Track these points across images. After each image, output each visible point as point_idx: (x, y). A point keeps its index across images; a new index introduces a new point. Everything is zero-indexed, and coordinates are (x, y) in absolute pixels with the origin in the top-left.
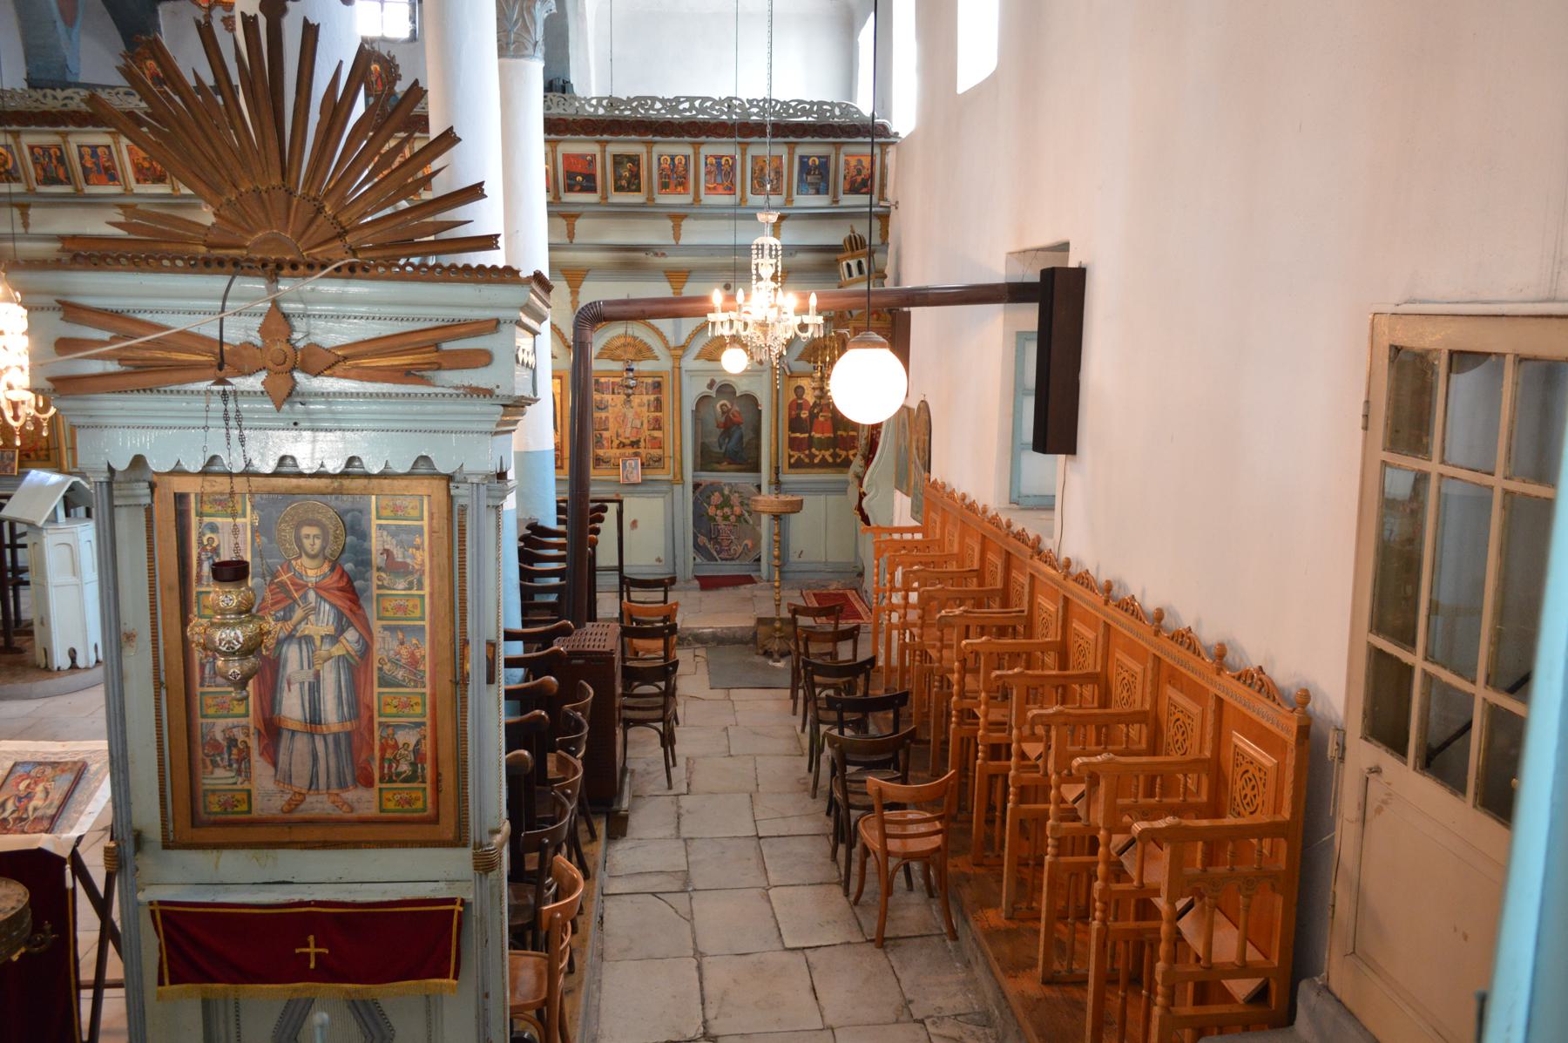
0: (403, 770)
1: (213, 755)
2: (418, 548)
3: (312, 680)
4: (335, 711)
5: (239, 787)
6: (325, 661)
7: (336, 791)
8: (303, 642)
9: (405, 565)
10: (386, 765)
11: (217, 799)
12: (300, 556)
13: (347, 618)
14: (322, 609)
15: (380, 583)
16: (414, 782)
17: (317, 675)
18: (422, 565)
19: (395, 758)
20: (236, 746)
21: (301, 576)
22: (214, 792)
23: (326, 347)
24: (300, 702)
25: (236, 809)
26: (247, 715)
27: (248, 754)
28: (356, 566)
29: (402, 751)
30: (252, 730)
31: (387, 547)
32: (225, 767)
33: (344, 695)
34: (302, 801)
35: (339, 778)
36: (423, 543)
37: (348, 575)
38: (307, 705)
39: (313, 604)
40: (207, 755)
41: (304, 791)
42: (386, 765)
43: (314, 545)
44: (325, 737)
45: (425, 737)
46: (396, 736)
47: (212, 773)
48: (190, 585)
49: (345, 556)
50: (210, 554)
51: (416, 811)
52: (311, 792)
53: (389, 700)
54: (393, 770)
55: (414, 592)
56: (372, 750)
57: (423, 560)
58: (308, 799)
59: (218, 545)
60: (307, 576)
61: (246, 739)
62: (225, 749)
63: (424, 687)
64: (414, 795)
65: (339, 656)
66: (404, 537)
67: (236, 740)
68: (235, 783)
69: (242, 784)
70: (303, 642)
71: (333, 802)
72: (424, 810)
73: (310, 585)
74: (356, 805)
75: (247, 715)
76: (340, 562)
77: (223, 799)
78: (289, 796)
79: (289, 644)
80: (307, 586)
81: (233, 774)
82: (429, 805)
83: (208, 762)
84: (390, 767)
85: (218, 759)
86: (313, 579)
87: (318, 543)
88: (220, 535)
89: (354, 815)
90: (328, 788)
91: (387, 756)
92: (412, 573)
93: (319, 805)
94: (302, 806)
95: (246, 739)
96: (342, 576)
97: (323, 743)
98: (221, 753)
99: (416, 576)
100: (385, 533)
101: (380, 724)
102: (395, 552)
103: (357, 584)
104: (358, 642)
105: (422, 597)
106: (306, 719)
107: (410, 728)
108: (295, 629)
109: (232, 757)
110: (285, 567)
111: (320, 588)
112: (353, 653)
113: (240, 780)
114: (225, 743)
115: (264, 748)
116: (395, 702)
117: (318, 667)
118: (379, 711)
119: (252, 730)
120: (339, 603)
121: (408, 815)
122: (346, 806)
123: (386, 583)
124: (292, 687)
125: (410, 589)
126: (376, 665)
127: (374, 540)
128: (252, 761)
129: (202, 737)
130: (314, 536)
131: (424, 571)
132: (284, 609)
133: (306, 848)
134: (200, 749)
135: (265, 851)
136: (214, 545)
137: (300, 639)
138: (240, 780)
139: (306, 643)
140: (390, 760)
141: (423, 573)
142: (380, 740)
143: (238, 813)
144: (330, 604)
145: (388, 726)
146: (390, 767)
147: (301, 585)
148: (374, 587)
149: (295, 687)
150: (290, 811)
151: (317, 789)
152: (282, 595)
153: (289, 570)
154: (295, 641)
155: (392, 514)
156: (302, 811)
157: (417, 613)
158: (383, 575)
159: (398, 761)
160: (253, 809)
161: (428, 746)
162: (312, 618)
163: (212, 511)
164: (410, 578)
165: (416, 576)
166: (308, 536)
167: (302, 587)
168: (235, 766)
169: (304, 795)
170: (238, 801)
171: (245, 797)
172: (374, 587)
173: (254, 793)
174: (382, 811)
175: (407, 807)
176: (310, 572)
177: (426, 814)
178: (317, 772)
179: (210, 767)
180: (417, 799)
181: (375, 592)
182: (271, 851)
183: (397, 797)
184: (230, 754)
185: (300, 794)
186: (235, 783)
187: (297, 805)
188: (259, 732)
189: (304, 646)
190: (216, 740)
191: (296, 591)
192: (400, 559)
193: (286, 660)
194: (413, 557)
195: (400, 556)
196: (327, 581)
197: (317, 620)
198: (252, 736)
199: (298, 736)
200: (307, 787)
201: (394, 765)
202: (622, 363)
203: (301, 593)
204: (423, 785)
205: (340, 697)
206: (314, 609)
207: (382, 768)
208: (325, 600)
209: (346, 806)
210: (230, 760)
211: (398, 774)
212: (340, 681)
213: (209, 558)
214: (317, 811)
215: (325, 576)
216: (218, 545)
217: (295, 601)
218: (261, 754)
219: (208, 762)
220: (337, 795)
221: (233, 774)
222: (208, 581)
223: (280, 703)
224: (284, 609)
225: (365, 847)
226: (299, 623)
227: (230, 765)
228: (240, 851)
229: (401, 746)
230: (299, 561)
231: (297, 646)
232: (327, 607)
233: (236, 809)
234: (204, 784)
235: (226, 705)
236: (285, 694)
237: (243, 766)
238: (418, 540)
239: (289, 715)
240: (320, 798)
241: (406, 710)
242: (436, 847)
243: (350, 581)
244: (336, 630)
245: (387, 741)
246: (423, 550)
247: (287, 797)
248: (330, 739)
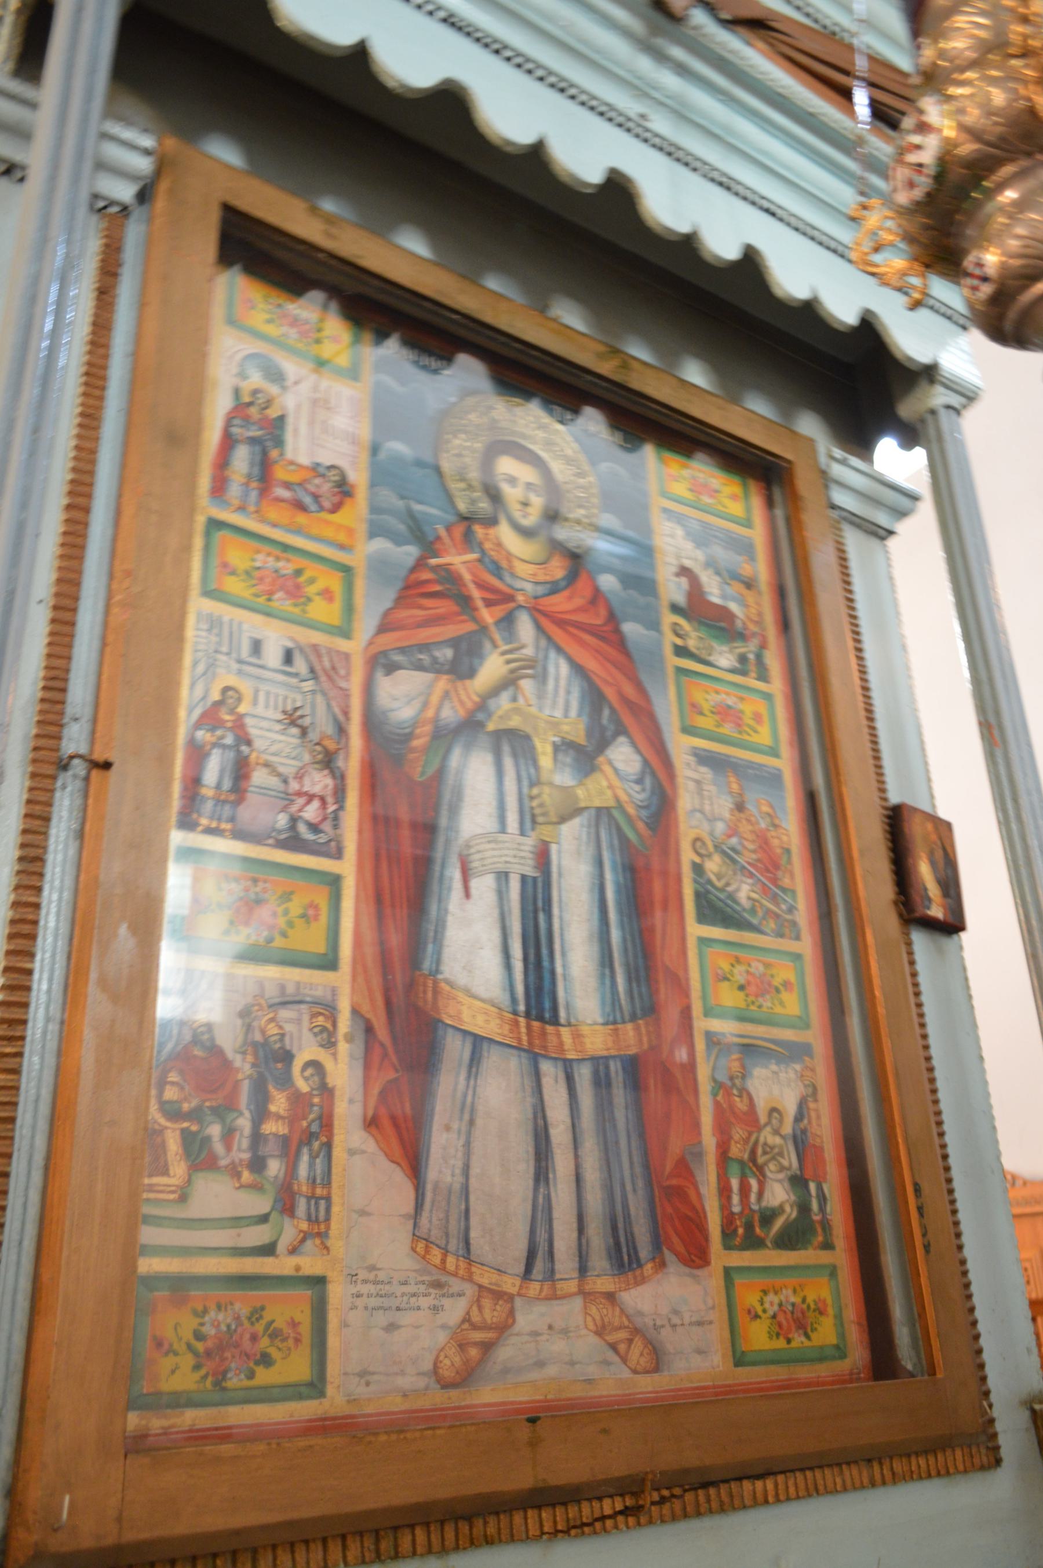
3: (530, 871)
5: (282, 1265)
17: (543, 857)
20: (285, 1081)
24: (496, 935)
25: (264, 1376)
33: (615, 935)
34: (504, 1327)
41: (510, 1284)
67: (287, 1057)
68: (268, 1250)
71: (600, 1332)
75: (329, 963)
79: (468, 747)
80: (510, 598)
85: (215, 1130)
93: (558, 1346)
98: (225, 1110)
103: (629, 628)
104: (639, 781)
112: (631, 810)
114: (244, 1066)
119: (344, 1007)
126: (688, 856)
132: (454, 643)
137: (499, 735)
138: (289, 1233)
144: (578, 668)
149: (484, 886)
151: (550, 1275)
167: (500, 598)
168: (275, 1167)
172: (668, 651)
176: (523, 570)
179: (178, 1170)
184: (261, 1114)
187: (487, 1347)
189: (508, 762)
199: (492, 1058)
206: (531, 663)
208: (559, 650)
210: (257, 1138)
215: (554, 589)
217: (484, 629)
219: (173, 1144)
220: (611, 1297)
227: (258, 1164)
233: (264, 1376)
247: (454, 1311)
248: (584, 1074)
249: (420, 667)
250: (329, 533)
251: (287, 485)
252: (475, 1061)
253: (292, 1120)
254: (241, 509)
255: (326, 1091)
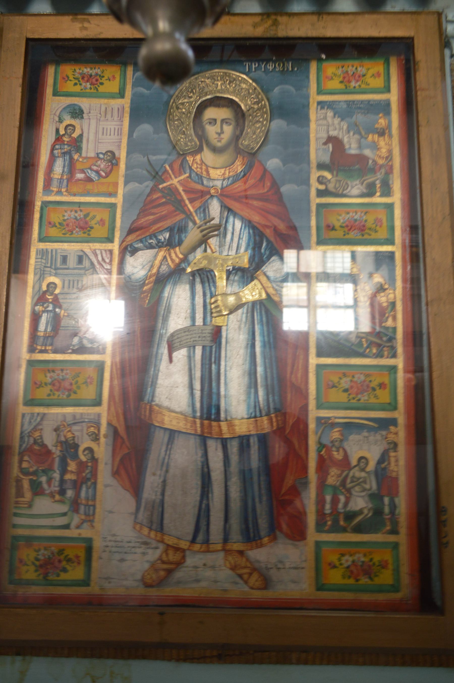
0: (357, 508)
1: (35, 473)
2: (382, 133)
4: (243, 397)
6: (231, 312)
7: (237, 547)
8: (198, 280)
9: (362, 159)
10: (328, 498)
11: (33, 555)
12: (200, 150)
13: (269, 242)
14: (230, 228)
15: (322, 187)
16: (376, 531)
18: (389, 157)
19: (343, 483)
20: (75, 456)
21: (200, 177)
22: (29, 540)
23: (140, 253)
24: (186, 379)
26: (98, 403)
27: (94, 473)
28: (285, 162)
29: (356, 473)
30: (104, 429)
31: (333, 133)
32: (52, 495)
33: (260, 370)
34: (179, 564)
35: (246, 520)
36: (389, 126)
37: (272, 175)
38: (197, 386)
39: (216, 221)
40: (25, 472)
41: (184, 545)
42: (328, 498)
43: (222, 132)
44: (224, 443)
45: (395, 445)
46: (346, 445)
47: (30, 506)
48: (42, 94)
49: (268, 148)
50: (66, 148)
51: (380, 589)
52: (197, 547)
53: (335, 379)
54: (340, 506)
55: (377, 199)
56: (305, 468)
57: (390, 152)
58: (190, 561)
59: (81, 136)
60: (210, 179)
61: (93, 445)
62: (57, 460)
63: (394, 356)
64: (377, 558)
65: (254, 303)
66: (359, 118)
67: (76, 446)
68: (67, 527)
69: (78, 527)
70: (198, 280)
71: (233, 568)
72: (395, 588)
73: (212, 191)
74: (273, 573)
76: (260, 156)
77: (43, 554)
78: (158, 553)
79: (175, 284)
80: (209, 193)
81: (64, 508)
82: (405, 579)
83: (26, 484)
84: (335, 501)
85: (44, 479)
86: (219, 184)
87: (228, 130)
88: (85, 123)
89: (268, 594)
90: (226, 540)
91: (331, 480)
92: (373, 171)
93: (209, 573)
94: (179, 574)
95: (93, 445)
96: (262, 179)
97: (220, 454)
99: (380, 175)
100: (330, 114)
101: (319, 420)
102: (346, 140)
105: (390, 207)
106: (194, 411)
107: (370, 429)
108: (185, 259)
109: (68, 477)
110: (176, 166)
111: (227, 196)
113: (76, 520)
114: (56, 452)
115: (122, 461)
116: (345, 383)
117: (218, 321)
118: (318, 398)
119: (104, 429)
120: (256, 218)
121: (366, 597)
122: (255, 576)
123: (331, 187)
124: (175, 354)
125: (371, 194)
127: (313, 125)
128: (99, 486)
129: (22, 438)
130: (223, 121)
131: (391, 167)
132: (171, 229)
133: (185, 660)
134: (16, 459)
135: (110, 662)
136: (75, 135)
138: (76, 520)
139: (202, 282)
140: (335, 488)
141: (390, 171)
142: (319, 451)
143: (65, 584)
144: (242, 219)
145: (333, 425)
146: (335, 501)
147: (202, 192)
148: (313, 192)
150: (160, 583)
151: (207, 541)
152: (170, 208)
153: (183, 167)
154: (185, 278)
155: (342, 86)
156: (179, 582)
157: (383, 234)
158: (327, 175)
159: (349, 491)
160: (94, 576)
161: (402, 462)
162: (213, 242)
163: (77, 89)
164: (370, 179)
165: (380, 175)
166: (213, 122)
168: (70, 493)
169: (184, 551)
170: (69, 560)
171: (82, 554)
172: (313, 192)
173: (97, 544)
174: (320, 587)
175: (364, 580)
176: (214, 173)
177: (398, 596)
178: (208, 506)
179: (28, 495)
180: (383, 565)
181: (315, 200)
182: (121, 662)
183: (347, 560)
184: (64, 471)
185: (177, 549)
186: (67, 527)
187: (169, 572)
188: (116, 432)
189: (199, 288)
190: (44, 446)
191: (192, 201)
192: (353, 150)
193: (168, 310)
194: (375, 147)
195: (354, 145)
196: (239, 186)
197: (221, 245)
198: (103, 440)
199: (179, 441)
200: (190, 537)
201: (342, 499)
202: (194, 550)
203: (198, 204)
204: (392, 538)
205: (252, 373)
206: (217, 227)
207: (320, 502)
209: (255, 576)
210: (62, 481)
211: (350, 516)
212: (253, 346)
213: (64, 154)
214: (204, 584)
215: (236, 178)
216: (81, 136)
217: (189, 216)
218: (116, 474)
219: (26, 484)
220: (241, 553)
221: (64, 508)
222: (60, 187)
223: (154, 384)
224: (171, 229)
225: (299, 662)
226: (194, 249)
227: (62, 492)
228: (64, 660)
229: (354, 462)
230: (198, 157)
231: (188, 287)
232: (238, 224)
234: (14, 526)
235: (67, 384)
236: (164, 364)
237: (83, 494)
238: (382, 122)
239: (166, 403)
240: (209, 558)
241: (364, 398)
242: (404, 664)
243: (275, 186)
244: (252, 260)
245: (329, 450)
246: (390, 136)
248: (234, 448)
249: (151, 247)
250: (103, 189)
251: (83, 171)
252: (171, 441)
253: (79, 472)
254: (59, 193)
255: (94, 460)
